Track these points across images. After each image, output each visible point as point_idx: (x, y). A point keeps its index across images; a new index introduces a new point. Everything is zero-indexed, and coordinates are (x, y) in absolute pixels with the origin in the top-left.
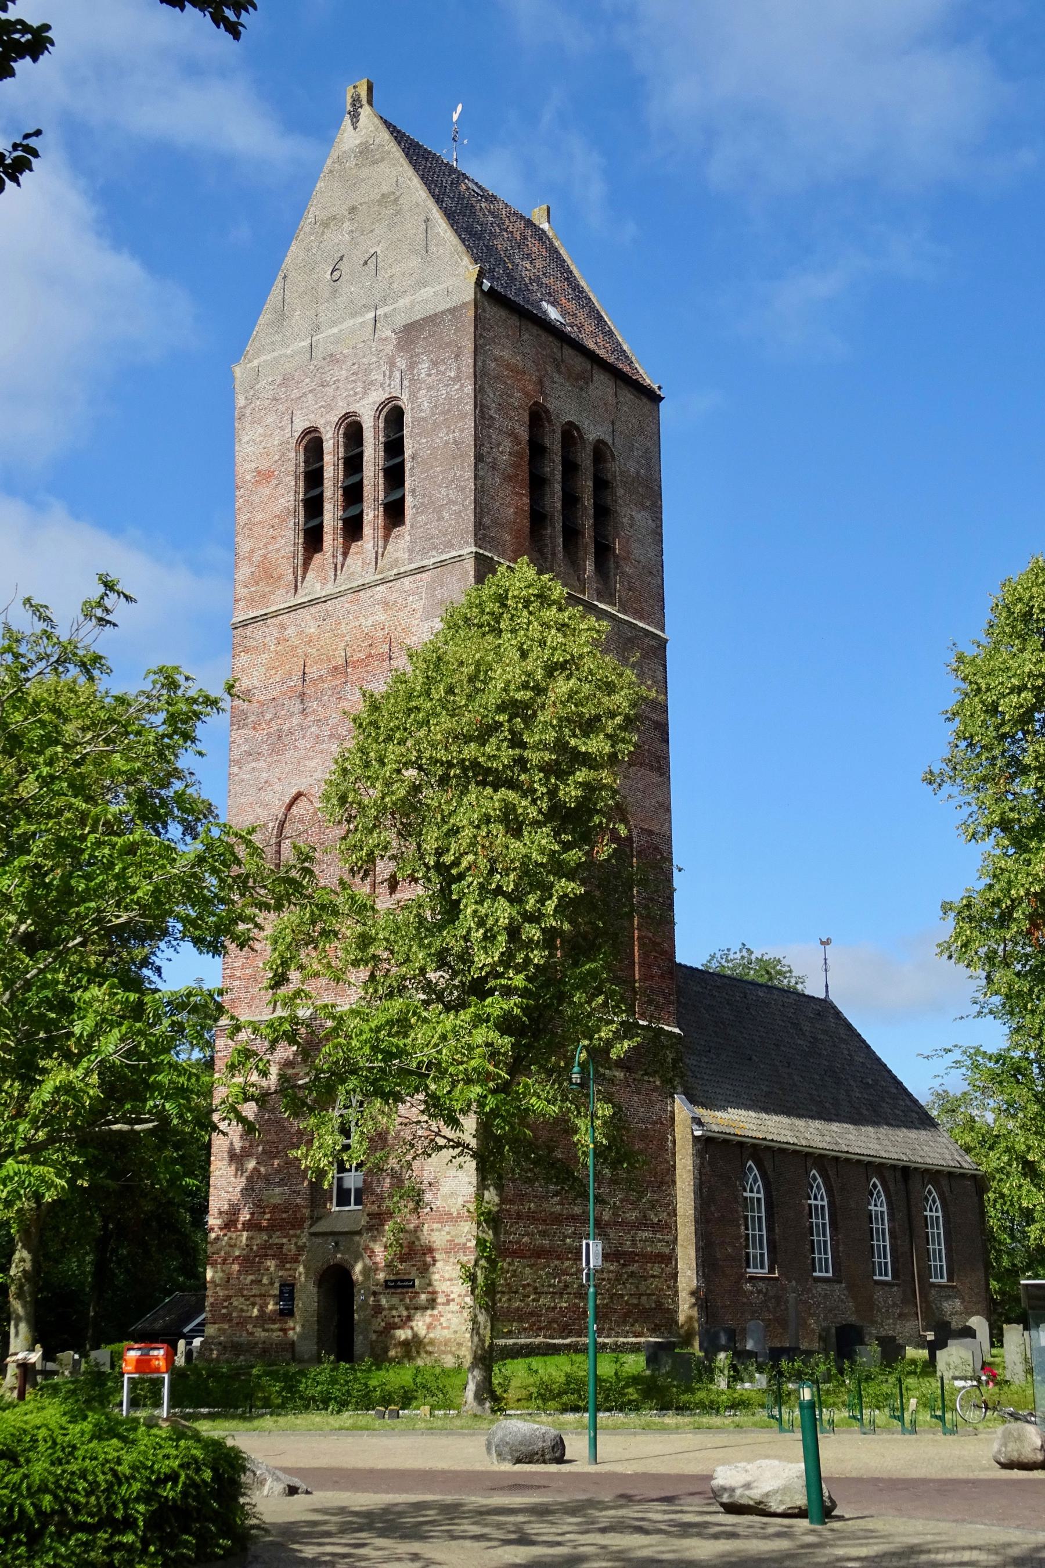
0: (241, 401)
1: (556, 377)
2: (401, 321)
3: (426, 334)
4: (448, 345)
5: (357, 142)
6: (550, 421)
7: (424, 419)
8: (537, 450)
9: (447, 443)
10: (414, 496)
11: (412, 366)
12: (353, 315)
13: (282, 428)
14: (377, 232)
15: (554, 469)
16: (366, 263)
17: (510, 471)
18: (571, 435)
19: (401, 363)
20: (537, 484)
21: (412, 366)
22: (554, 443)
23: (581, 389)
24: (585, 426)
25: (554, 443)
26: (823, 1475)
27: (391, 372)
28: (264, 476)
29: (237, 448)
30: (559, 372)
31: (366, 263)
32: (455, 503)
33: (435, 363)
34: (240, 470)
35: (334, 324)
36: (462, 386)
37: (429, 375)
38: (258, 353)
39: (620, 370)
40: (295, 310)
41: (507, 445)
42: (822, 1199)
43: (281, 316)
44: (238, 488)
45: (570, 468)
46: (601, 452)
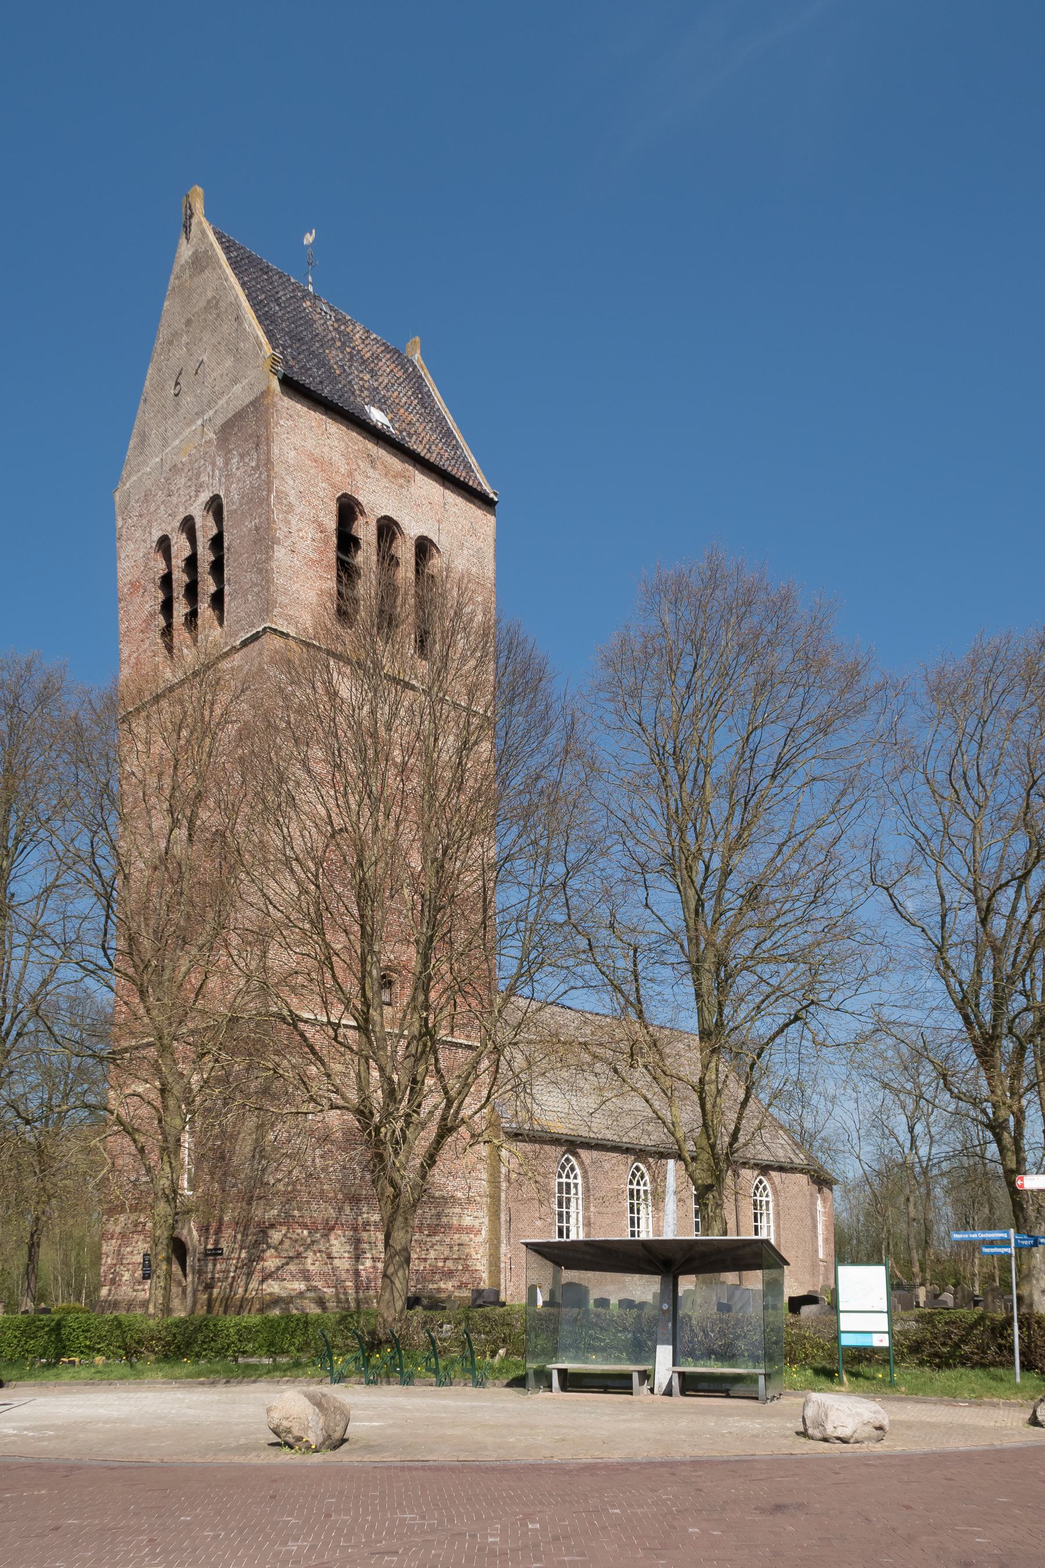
0: (120, 523)
1: (371, 472)
2: (220, 421)
3: (236, 429)
4: (251, 436)
5: (190, 253)
6: (362, 513)
7: (235, 511)
8: (347, 542)
9: (250, 530)
10: (229, 584)
11: (227, 462)
12: (188, 425)
13: (144, 541)
14: (204, 339)
15: (366, 557)
16: (196, 373)
17: (315, 556)
18: (387, 529)
19: (220, 462)
20: (346, 571)
21: (227, 462)
22: (406, 552)
23: (402, 486)
24: (406, 522)
25: (365, 531)
26: (671, 1347)
27: (213, 471)
28: (134, 586)
29: (119, 565)
30: (373, 467)
31: (196, 373)
32: (256, 585)
33: (242, 456)
34: (120, 584)
35: (177, 435)
36: (261, 473)
37: (238, 469)
38: (129, 476)
39: (297, 381)
40: (152, 430)
41: (310, 532)
42: (575, 1177)
43: (143, 438)
44: (120, 600)
45: (388, 560)
46: (424, 547)
